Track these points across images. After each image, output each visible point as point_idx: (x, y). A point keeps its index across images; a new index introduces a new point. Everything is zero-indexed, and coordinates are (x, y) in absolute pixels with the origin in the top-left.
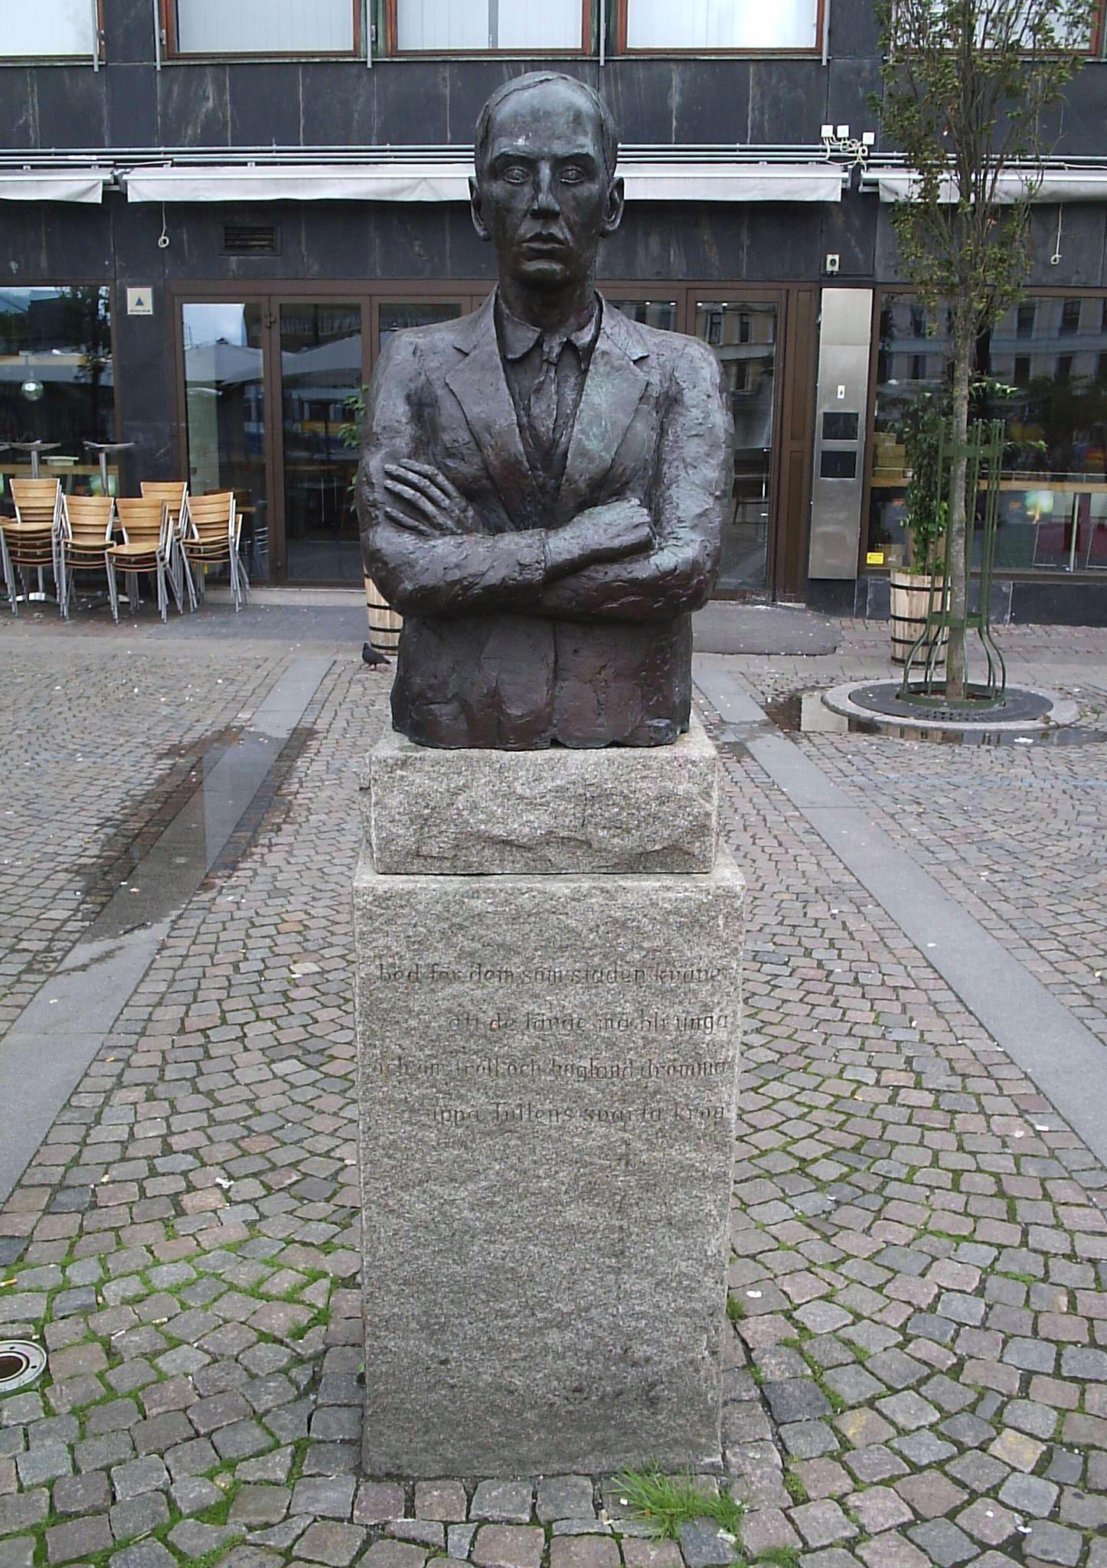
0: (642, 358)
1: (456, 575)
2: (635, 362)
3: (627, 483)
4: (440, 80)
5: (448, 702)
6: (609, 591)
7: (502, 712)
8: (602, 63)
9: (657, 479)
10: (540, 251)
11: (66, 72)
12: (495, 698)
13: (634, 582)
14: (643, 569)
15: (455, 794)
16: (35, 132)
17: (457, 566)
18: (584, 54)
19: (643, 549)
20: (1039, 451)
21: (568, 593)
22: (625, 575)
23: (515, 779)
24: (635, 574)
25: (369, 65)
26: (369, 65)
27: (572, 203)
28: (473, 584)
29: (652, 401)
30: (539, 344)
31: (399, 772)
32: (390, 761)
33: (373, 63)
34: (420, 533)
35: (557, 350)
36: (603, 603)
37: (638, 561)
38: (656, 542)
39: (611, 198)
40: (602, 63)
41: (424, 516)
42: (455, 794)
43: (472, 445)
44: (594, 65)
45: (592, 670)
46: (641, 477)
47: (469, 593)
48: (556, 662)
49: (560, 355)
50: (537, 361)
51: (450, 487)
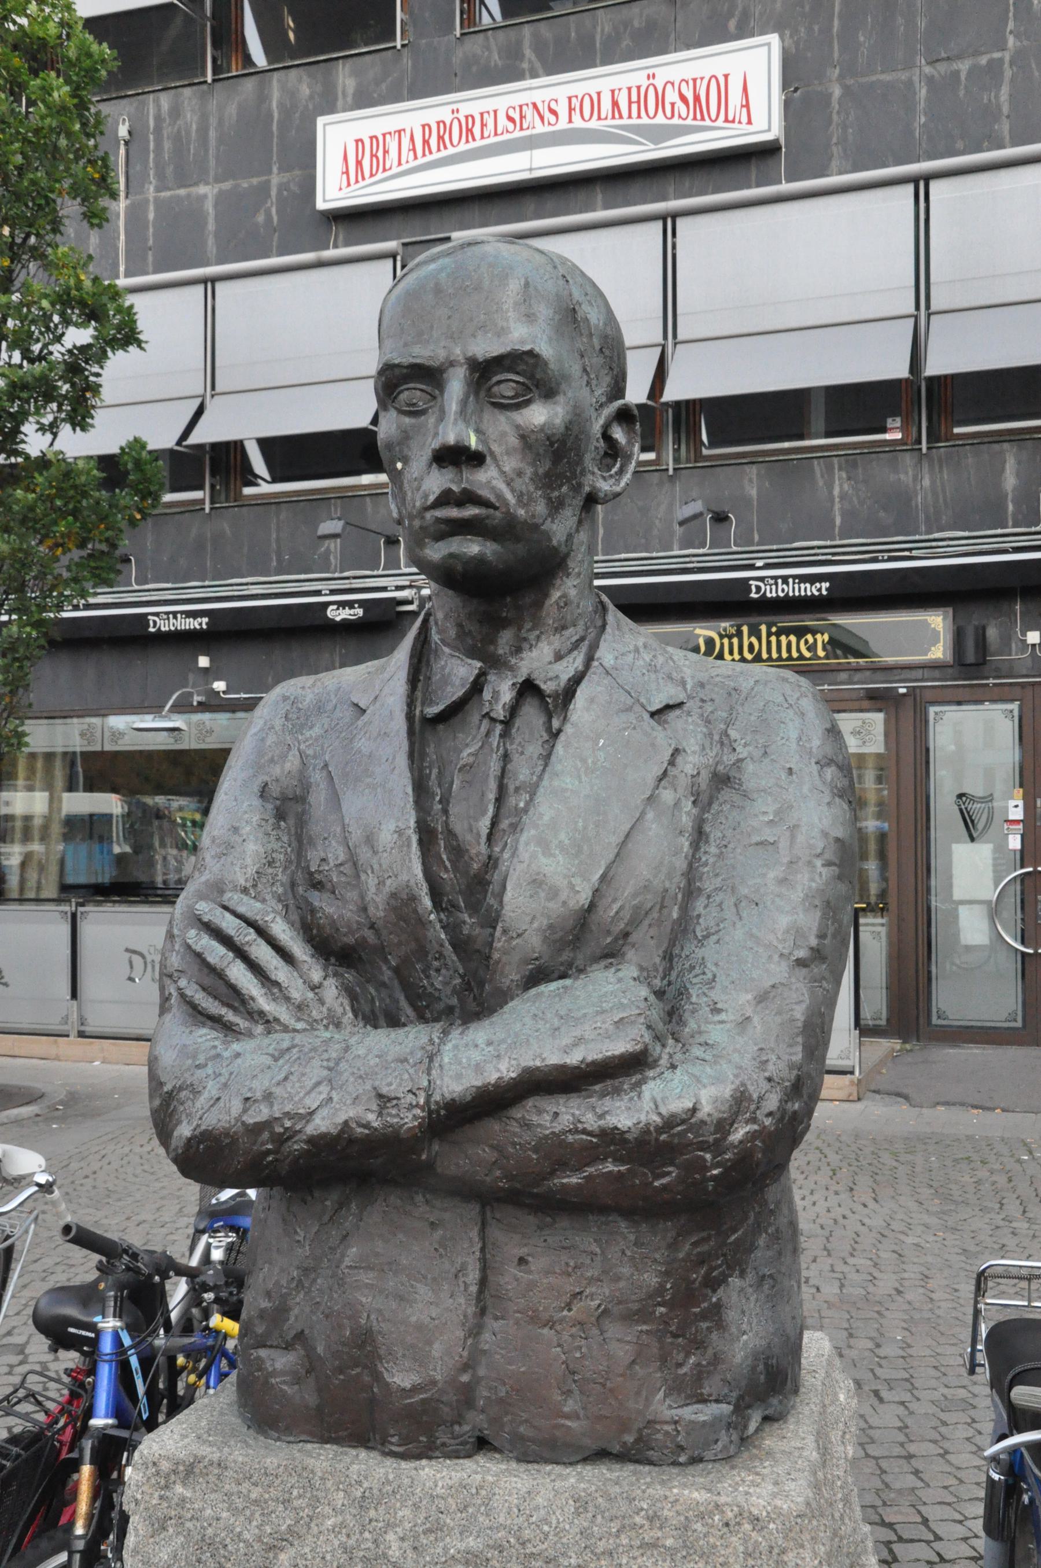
0: (668, 707)
1: (260, 1114)
2: (653, 715)
3: (626, 935)
4: (746, 482)
5: (288, 1347)
6: (561, 1153)
7: (378, 1377)
8: (924, 450)
9: (682, 929)
10: (449, 521)
11: (368, 499)
12: (364, 1348)
13: (611, 1140)
14: (628, 1112)
15: (272, 1548)
16: (336, 558)
17: (268, 1097)
18: (906, 444)
19: (632, 1066)
20: (184, 1484)
21: (486, 1153)
22: (591, 1122)
23: (389, 1526)
24: (611, 1121)
25: (671, 472)
26: (671, 472)
27: (513, 441)
28: (289, 1135)
29: (683, 782)
30: (477, 687)
31: (179, 1489)
32: (165, 1466)
33: (675, 469)
34: (228, 1028)
35: (507, 696)
36: (553, 1173)
37: (617, 1091)
38: (662, 1055)
39: (606, 437)
40: (924, 450)
41: (235, 997)
42: (272, 1548)
43: (347, 869)
44: (916, 453)
45: (581, 1287)
46: (654, 930)
47: (286, 1148)
48: (483, 1282)
49: (514, 710)
50: (475, 718)
51: (299, 949)
